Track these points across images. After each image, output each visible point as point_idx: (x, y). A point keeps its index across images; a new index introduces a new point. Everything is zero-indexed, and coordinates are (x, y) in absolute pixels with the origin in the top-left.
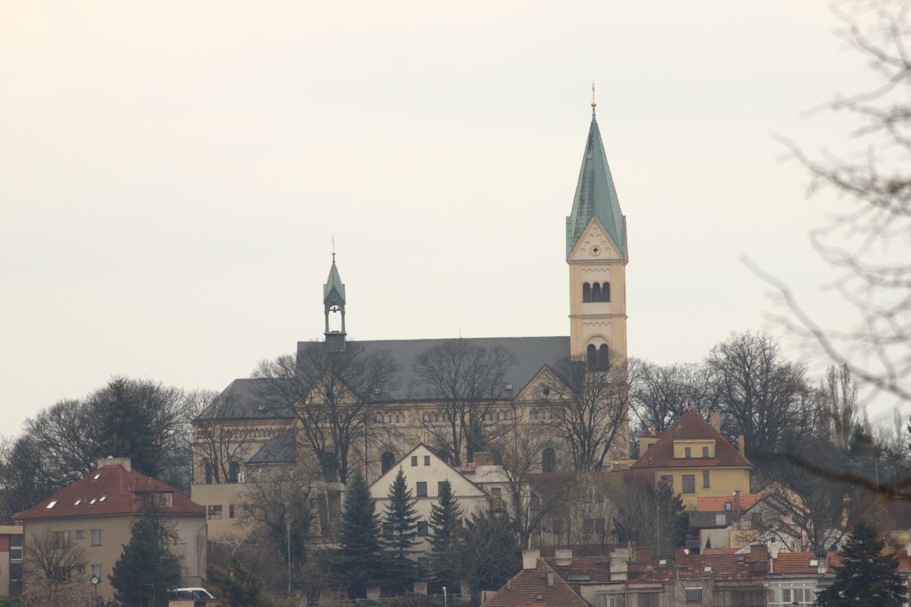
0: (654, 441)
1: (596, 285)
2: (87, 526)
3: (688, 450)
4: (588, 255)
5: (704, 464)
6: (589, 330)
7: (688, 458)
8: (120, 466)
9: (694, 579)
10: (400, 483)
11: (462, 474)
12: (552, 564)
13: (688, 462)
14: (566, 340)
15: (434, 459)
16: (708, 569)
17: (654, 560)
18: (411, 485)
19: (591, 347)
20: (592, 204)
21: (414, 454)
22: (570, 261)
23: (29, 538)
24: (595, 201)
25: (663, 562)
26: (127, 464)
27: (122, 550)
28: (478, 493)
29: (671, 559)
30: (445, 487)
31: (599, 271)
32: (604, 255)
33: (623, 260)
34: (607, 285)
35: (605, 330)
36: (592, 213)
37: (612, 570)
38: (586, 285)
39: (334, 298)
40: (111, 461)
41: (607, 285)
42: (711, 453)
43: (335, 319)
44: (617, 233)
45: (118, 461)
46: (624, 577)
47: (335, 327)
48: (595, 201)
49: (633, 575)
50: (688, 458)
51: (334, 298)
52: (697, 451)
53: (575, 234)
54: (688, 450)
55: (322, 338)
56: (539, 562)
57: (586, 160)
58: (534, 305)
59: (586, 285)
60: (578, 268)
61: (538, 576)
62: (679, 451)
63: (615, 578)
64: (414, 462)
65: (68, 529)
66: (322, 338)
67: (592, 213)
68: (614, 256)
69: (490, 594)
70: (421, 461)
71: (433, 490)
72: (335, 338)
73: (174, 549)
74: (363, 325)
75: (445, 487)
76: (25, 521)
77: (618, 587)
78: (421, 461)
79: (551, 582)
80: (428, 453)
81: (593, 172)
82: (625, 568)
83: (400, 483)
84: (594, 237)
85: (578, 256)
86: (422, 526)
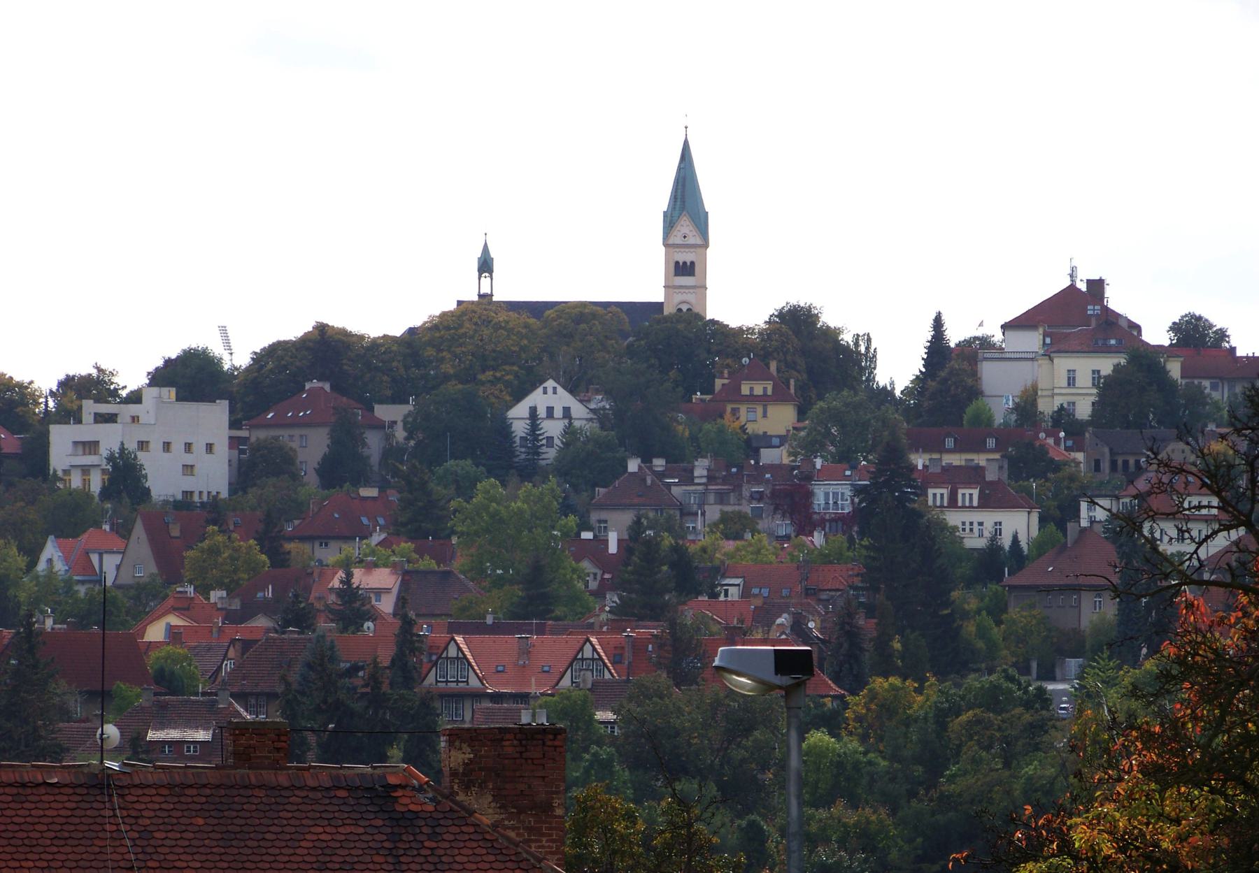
0: (726, 381)
1: (685, 263)
2: (297, 432)
3: (752, 389)
4: (679, 240)
5: (764, 400)
6: (678, 298)
7: (751, 395)
8: (322, 388)
9: (759, 483)
10: (533, 410)
11: (581, 401)
12: (650, 468)
13: (752, 398)
14: (658, 307)
15: (560, 390)
16: (768, 476)
17: (728, 468)
18: (542, 412)
19: (680, 310)
20: (683, 202)
21: (545, 385)
22: (666, 245)
23: (253, 439)
24: (685, 204)
25: (734, 470)
26: (327, 387)
27: (26, 380)
28: (591, 416)
29: (740, 468)
30: (567, 411)
31: (210, 869)
32: (691, 241)
33: (706, 245)
34: (692, 263)
35: (691, 297)
36: (683, 208)
37: (696, 474)
38: (677, 263)
39: (485, 266)
40: (315, 383)
41: (692, 263)
42: (769, 392)
43: (485, 282)
44: (701, 222)
45: (320, 384)
46: (704, 480)
47: (485, 289)
48: (685, 204)
49: (711, 478)
50: (751, 395)
51: (485, 266)
52: (758, 390)
53: (670, 222)
54: (752, 389)
55: (476, 298)
56: (640, 467)
57: (679, 169)
58: (639, 279)
59: (677, 263)
60: (671, 250)
61: (639, 477)
62: (745, 390)
63: (696, 481)
64: (545, 392)
65: (283, 434)
66: (476, 298)
67: (683, 208)
68: (699, 241)
69: (602, 490)
70: (550, 391)
71: (558, 413)
72: (485, 298)
73: (366, 452)
74: (511, 286)
75: (567, 411)
76: (252, 427)
77: (700, 488)
78: (550, 391)
79: (649, 482)
80: (555, 385)
81: (684, 178)
82: (705, 473)
83: (533, 410)
84: (685, 227)
85: (671, 241)
86: (550, 439)
